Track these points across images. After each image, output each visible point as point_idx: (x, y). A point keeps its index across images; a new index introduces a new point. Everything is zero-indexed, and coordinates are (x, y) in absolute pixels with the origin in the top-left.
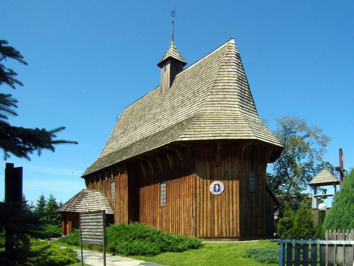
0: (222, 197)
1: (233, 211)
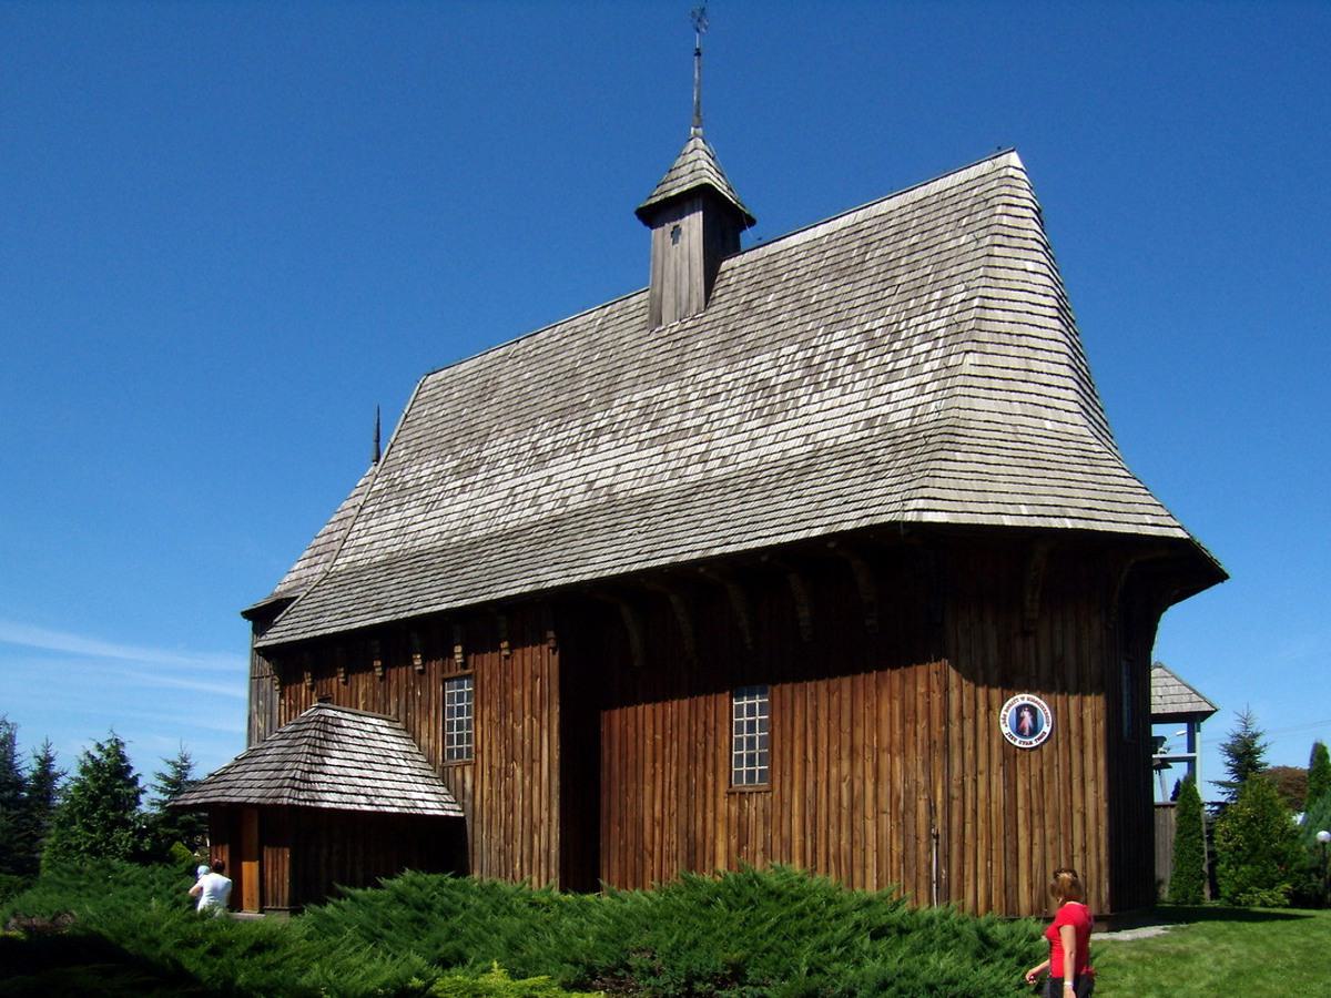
0: (1045, 758)
1: (1084, 815)
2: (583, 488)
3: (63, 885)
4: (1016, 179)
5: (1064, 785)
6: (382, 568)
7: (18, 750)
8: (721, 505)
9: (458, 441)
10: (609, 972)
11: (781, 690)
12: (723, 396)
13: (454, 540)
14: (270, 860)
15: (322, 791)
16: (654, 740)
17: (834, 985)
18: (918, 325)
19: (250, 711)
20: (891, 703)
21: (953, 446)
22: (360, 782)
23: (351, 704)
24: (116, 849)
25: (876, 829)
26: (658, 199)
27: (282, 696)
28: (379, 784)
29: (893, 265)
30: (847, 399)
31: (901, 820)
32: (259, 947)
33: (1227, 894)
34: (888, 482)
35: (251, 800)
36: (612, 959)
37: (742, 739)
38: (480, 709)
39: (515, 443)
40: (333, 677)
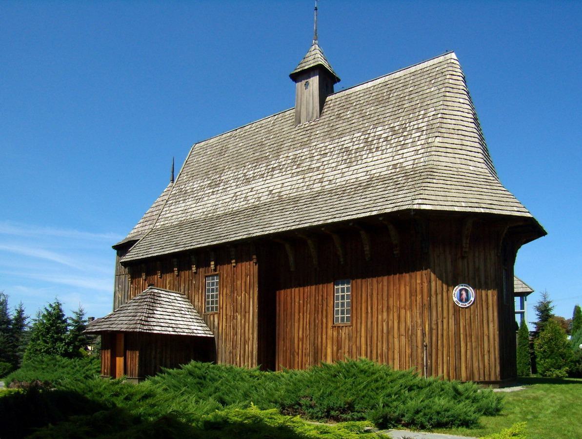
0: (472, 312)
1: (489, 337)
2: (267, 193)
3: (35, 367)
4: (455, 64)
5: (480, 323)
6: (177, 227)
7: (8, 307)
8: (330, 201)
9: (210, 173)
10: (291, 406)
11: (356, 282)
12: (329, 154)
13: (210, 215)
14: (130, 356)
15: (154, 326)
16: (299, 303)
17: (394, 412)
18: (414, 125)
19: (115, 290)
20: (405, 287)
21: (432, 177)
22: (170, 321)
23: (164, 287)
24: (57, 351)
25: (399, 343)
26: (299, 70)
27: (132, 283)
28: (178, 322)
29: (402, 99)
30: (384, 156)
31: (410, 339)
32: (146, 397)
33: (540, 372)
34: (405, 192)
35: (123, 330)
36: (293, 400)
37: (339, 303)
38: (222, 289)
39: (236, 174)
40: (155, 275)
